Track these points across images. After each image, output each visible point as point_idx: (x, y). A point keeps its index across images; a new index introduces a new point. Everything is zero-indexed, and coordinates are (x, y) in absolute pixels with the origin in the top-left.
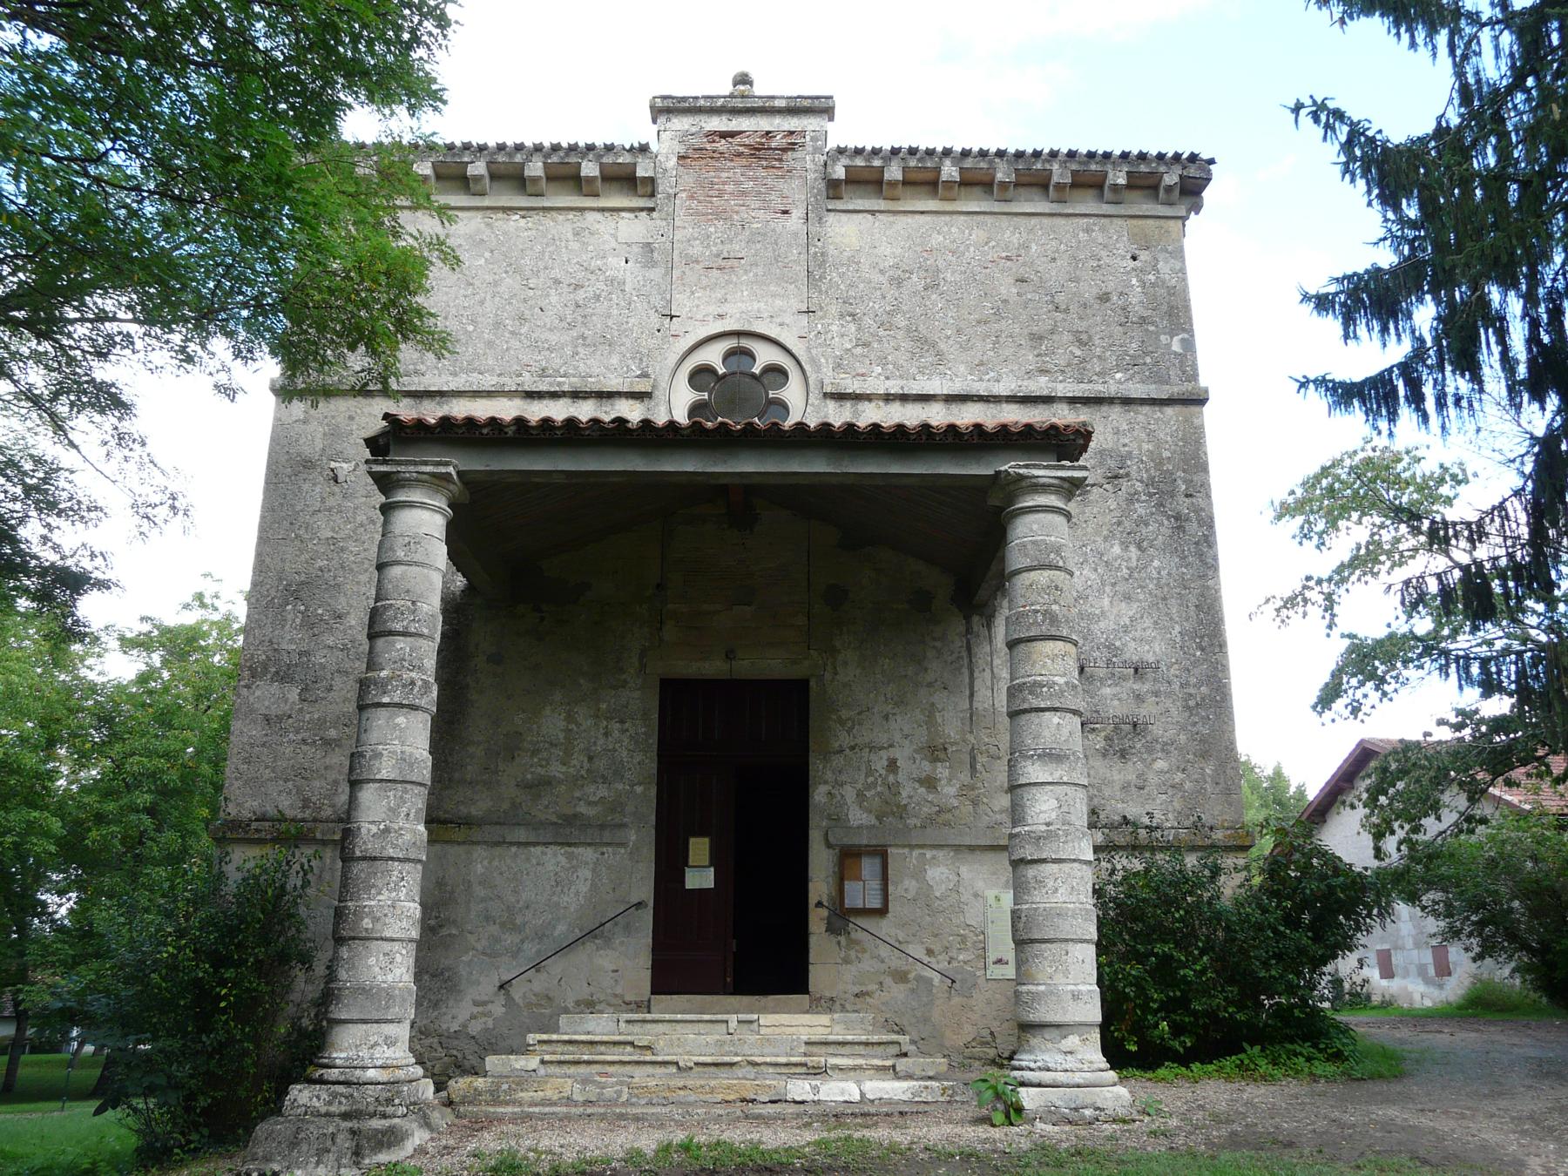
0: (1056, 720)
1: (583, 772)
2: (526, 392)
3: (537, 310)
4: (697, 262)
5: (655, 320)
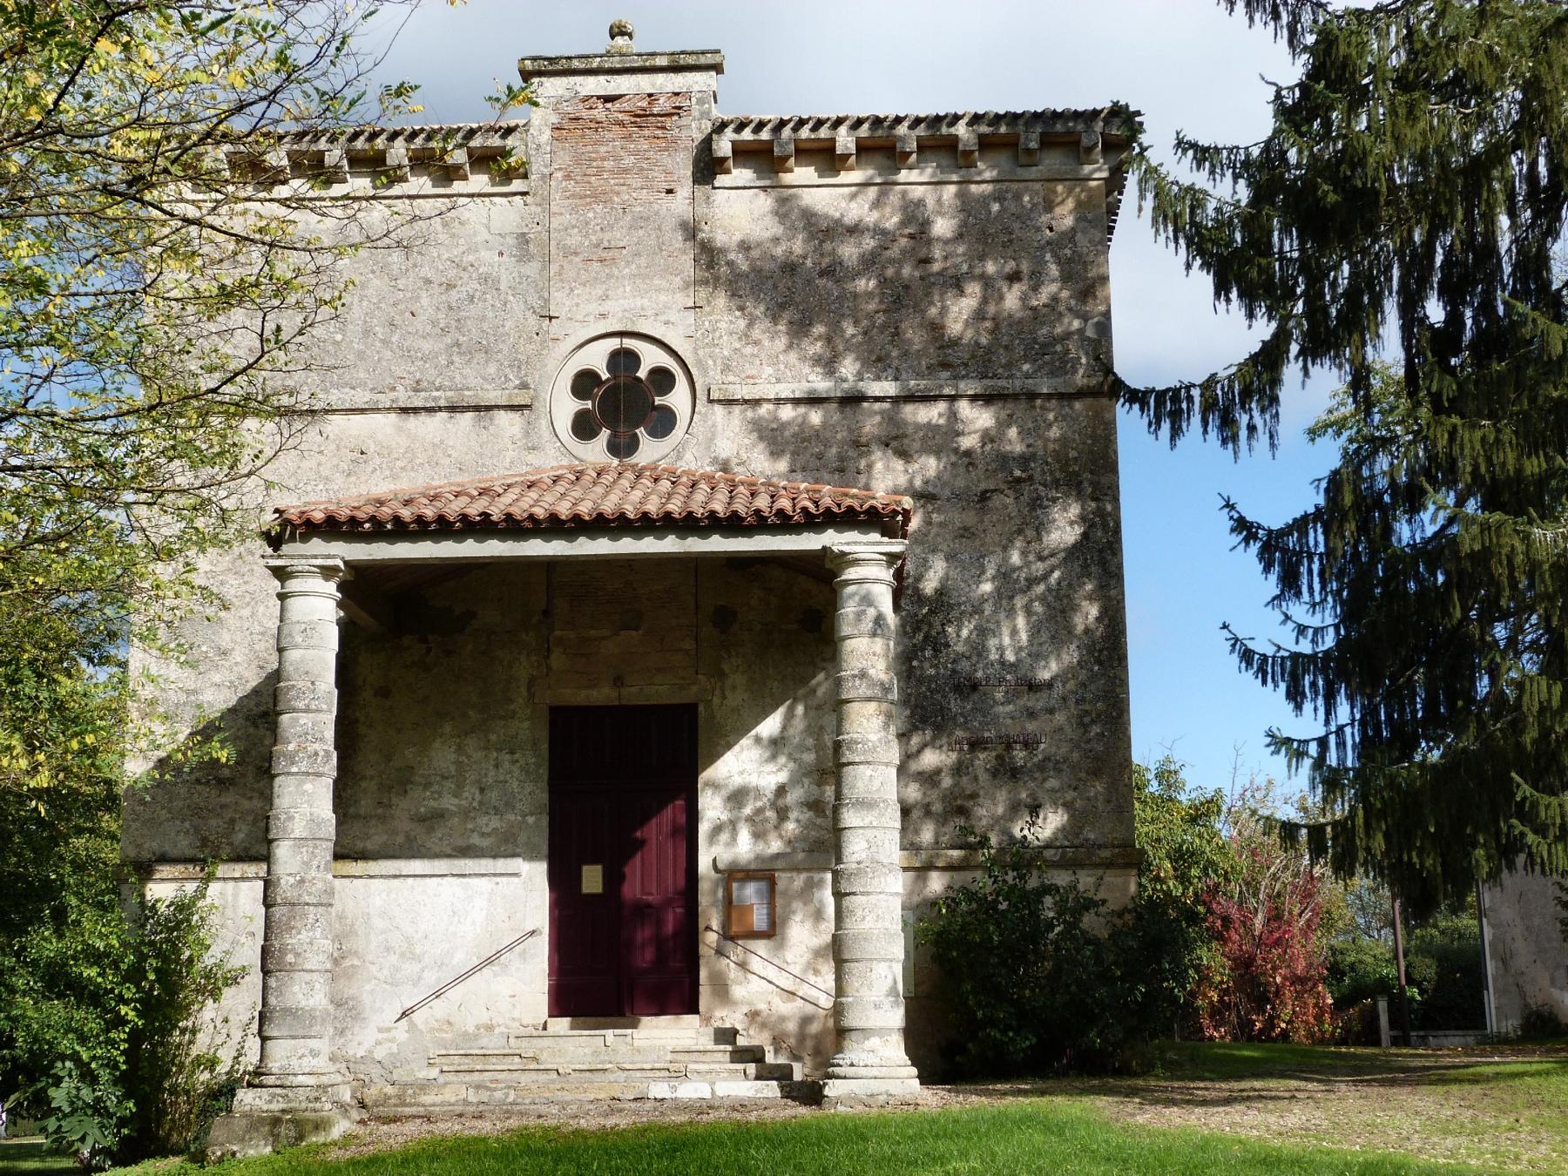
0: (869, 772)
1: (475, 804)
2: (401, 409)
3: (408, 314)
4: (576, 254)
5: (533, 320)
